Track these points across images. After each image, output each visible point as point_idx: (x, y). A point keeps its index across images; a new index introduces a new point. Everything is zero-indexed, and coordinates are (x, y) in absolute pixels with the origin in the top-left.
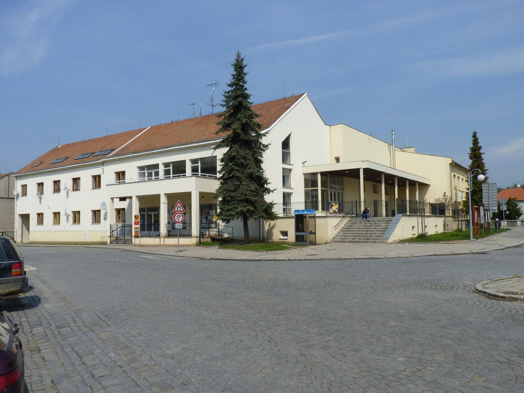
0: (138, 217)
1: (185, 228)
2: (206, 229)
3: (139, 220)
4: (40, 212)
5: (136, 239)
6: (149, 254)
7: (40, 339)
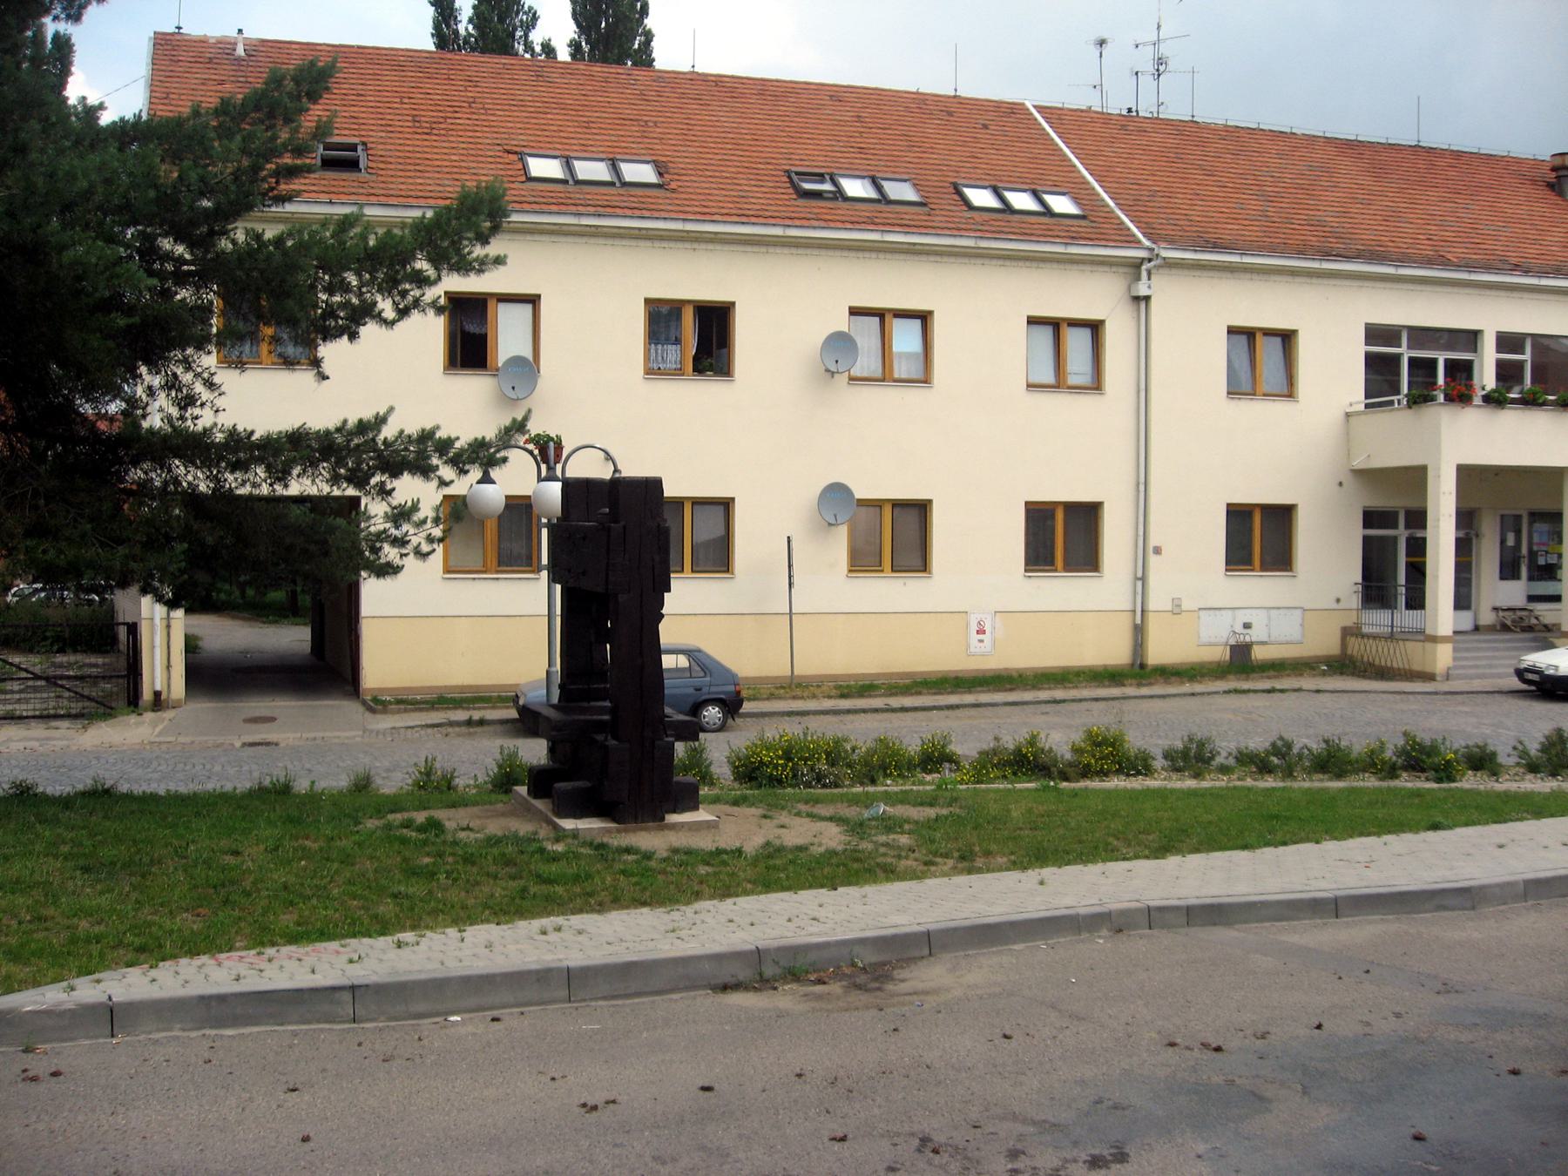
6: (1251, 694)
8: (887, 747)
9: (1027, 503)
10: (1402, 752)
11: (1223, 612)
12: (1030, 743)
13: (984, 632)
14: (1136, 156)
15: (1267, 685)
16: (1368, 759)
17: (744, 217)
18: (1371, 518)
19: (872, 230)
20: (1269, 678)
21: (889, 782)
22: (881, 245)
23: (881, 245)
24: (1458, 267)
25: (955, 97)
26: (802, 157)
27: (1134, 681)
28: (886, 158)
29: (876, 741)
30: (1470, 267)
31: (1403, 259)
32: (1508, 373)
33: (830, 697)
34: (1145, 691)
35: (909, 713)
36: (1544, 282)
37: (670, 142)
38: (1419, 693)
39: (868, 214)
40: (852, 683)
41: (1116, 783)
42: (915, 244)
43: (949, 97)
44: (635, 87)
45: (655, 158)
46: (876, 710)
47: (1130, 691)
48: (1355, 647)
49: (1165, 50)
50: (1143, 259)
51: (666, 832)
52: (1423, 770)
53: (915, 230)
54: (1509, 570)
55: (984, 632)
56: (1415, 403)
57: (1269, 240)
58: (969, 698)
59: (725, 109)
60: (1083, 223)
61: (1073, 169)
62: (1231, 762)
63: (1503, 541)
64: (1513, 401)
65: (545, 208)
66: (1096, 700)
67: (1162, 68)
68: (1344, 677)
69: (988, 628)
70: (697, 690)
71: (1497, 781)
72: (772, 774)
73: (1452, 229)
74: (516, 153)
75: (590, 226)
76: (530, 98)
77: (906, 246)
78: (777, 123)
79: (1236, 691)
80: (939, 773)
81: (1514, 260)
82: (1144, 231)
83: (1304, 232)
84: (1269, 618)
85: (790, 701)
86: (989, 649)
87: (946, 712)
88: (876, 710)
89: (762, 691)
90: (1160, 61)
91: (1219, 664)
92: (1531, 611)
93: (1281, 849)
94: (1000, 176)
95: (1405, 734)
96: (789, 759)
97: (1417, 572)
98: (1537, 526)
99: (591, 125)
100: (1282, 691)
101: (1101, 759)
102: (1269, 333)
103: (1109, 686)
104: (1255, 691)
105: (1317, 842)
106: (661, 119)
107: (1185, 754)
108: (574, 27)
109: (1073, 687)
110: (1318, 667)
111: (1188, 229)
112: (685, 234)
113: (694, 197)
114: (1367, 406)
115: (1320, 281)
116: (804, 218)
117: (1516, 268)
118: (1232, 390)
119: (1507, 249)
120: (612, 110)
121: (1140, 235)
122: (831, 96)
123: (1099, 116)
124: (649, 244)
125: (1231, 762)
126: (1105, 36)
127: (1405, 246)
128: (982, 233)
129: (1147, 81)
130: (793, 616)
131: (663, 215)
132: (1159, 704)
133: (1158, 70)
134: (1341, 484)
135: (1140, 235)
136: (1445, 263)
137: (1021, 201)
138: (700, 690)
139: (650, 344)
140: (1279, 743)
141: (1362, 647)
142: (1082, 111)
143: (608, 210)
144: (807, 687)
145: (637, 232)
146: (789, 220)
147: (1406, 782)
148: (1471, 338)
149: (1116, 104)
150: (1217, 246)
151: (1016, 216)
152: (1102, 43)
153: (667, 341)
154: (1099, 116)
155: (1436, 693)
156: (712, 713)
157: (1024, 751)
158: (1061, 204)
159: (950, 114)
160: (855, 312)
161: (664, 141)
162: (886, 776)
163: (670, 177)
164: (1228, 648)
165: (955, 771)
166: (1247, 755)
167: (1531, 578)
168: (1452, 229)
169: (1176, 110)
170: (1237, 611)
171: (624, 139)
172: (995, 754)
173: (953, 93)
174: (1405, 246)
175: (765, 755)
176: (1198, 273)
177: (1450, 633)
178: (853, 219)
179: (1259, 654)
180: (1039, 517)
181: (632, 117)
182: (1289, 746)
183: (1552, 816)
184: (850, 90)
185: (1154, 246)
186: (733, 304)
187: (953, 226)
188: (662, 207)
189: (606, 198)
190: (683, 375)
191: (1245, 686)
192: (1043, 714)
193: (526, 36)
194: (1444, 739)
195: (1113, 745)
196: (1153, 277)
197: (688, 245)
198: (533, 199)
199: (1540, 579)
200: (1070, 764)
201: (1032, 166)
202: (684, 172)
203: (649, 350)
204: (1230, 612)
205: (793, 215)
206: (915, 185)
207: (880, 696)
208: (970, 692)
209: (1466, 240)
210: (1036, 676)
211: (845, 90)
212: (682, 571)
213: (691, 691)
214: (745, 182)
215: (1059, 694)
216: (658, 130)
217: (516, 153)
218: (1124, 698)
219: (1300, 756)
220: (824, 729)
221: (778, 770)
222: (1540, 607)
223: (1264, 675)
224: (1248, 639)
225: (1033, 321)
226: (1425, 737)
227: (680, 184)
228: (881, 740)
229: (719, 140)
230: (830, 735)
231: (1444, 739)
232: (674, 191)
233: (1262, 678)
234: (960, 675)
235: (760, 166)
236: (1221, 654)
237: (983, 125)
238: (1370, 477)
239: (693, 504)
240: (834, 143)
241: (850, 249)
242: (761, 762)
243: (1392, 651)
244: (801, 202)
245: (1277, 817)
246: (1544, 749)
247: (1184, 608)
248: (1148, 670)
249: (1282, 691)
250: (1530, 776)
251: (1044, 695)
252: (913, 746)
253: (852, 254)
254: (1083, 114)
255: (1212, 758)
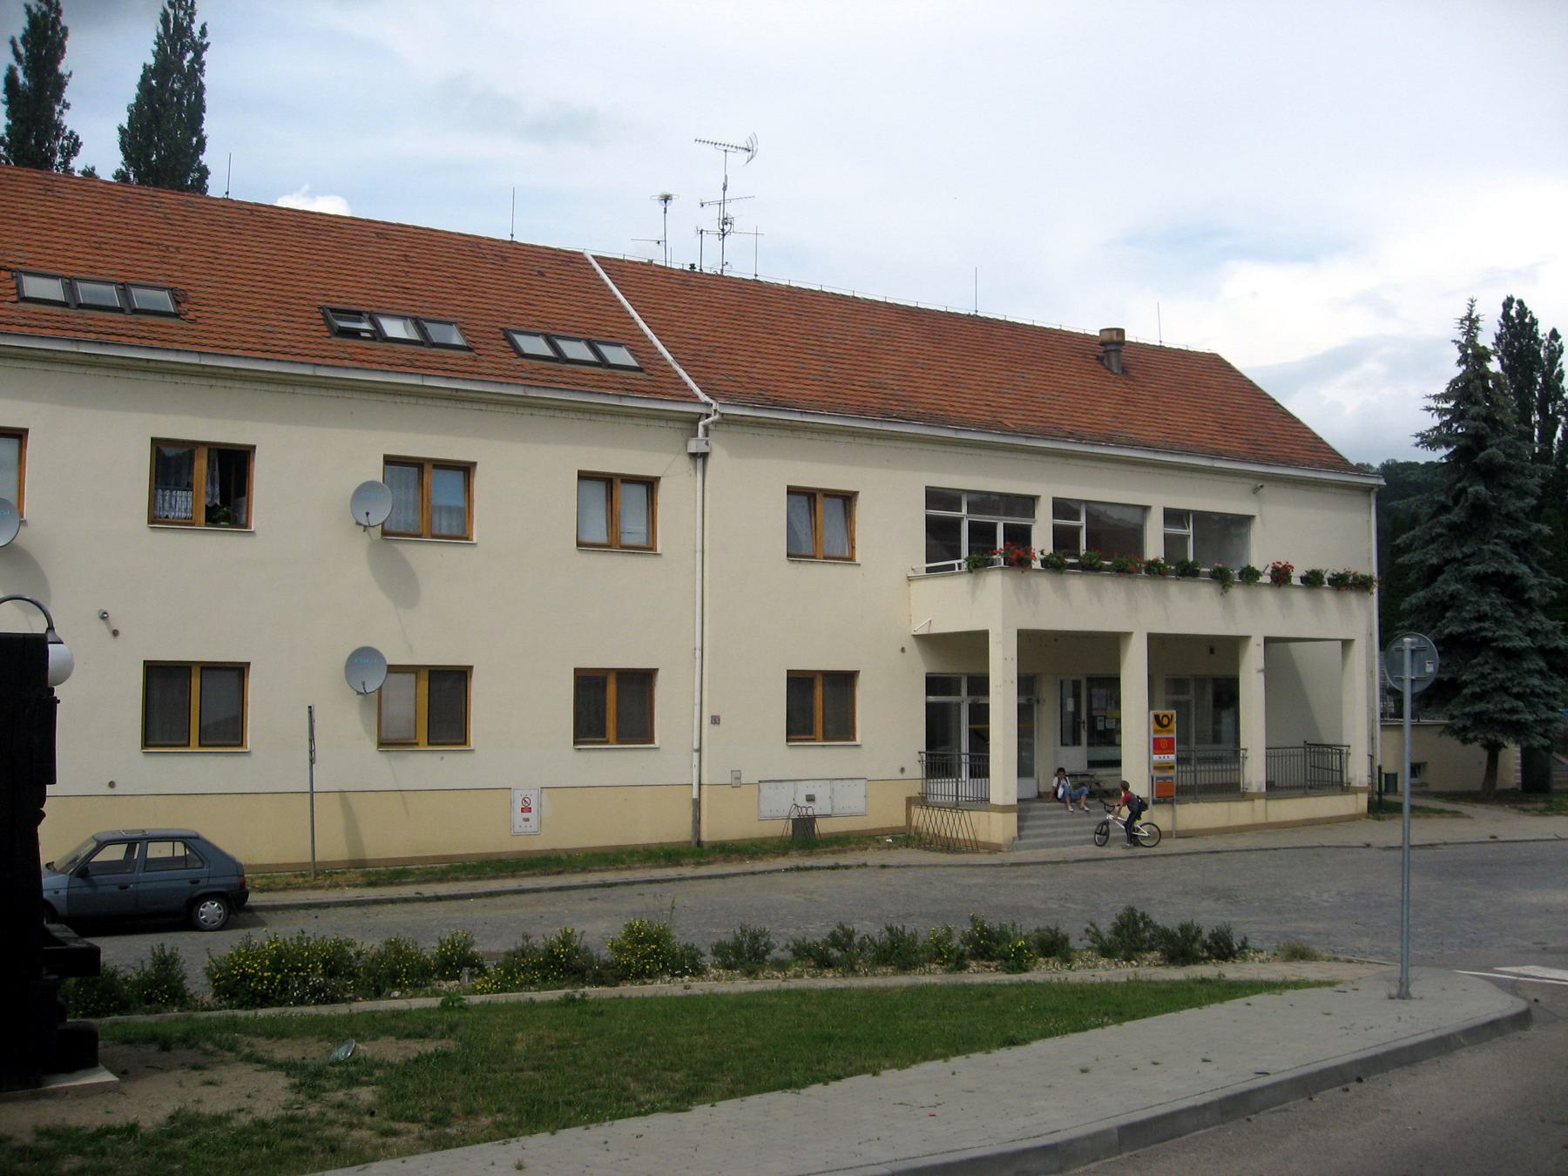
0: (1170, 720)
1: (1185, 759)
2: (1216, 762)
3: (1170, 731)
4: (716, 727)
5: (1556, 787)
6: (814, 873)
7: (861, 1166)
8: (399, 952)
9: (576, 670)
10: (969, 939)
11: (785, 784)
12: (562, 942)
13: (529, 810)
14: (698, 312)
15: (829, 860)
16: (934, 949)
17: (269, 354)
18: (934, 684)
19: (411, 373)
20: (833, 853)
21: (396, 993)
22: (420, 390)
23: (420, 390)
24: (1015, 434)
25: (512, 242)
26: (340, 294)
27: (692, 861)
28: (432, 300)
29: (386, 943)
30: (1028, 434)
31: (964, 425)
32: (1064, 539)
33: (355, 886)
34: (703, 871)
35: (444, 903)
36: (1097, 450)
37: (193, 270)
38: (986, 865)
39: (409, 357)
40: (383, 869)
41: (665, 987)
42: (457, 390)
43: (504, 242)
44: (160, 210)
45: (172, 285)
46: (406, 900)
47: (687, 871)
48: (920, 817)
49: (730, 210)
50: (701, 414)
51: (43, 1101)
52: (991, 959)
53: (460, 375)
54: (1070, 736)
55: (529, 810)
56: (976, 567)
57: (830, 400)
58: (511, 884)
59: (258, 239)
60: (639, 375)
61: (631, 321)
62: (787, 955)
63: (1062, 706)
64: (1072, 566)
65: (37, 331)
66: (650, 882)
67: (727, 228)
68: (910, 850)
69: (534, 806)
70: (192, 882)
71: (1070, 968)
72: (256, 989)
73: (1009, 396)
74: (9, 270)
75: (90, 354)
76: (35, 213)
77: (448, 392)
78: (316, 258)
79: (798, 869)
80: (459, 979)
81: (1068, 428)
82: (701, 386)
83: (865, 394)
84: (833, 790)
85: (309, 892)
86: (535, 828)
87: (487, 901)
88: (406, 900)
89: (277, 880)
90: (725, 221)
91: (781, 839)
92: (1092, 776)
93: (834, 1085)
94: (553, 324)
95: (973, 919)
96: (279, 971)
97: (980, 739)
98: (1095, 691)
99: (103, 246)
100: (847, 867)
101: (643, 958)
102: (830, 494)
103: (666, 866)
104: (819, 868)
105: (875, 1074)
106: (184, 245)
107: (737, 949)
108: (120, 157)
109: (626, 869)
110: (884, 840)
111: (748, 386)
112: (200, 369)
113: (214, 329)
114: (928, 570)
115: (881, 442)
116: (336, 358)
117: (1069, 436)
118: (793, 552)
119: (1062, 417)
120: (129, 232)
121: (697, 390)
122: (377, 234)
123: (662, 270)
124: (158, 377)
125: (787, 955)
126: (668, 192)
127: (964, 411)
128: (530, 382)
129: (712, 241)
130: (308, 790)
131: (177, 346)
132: (718, 883)
133: (723, 230)
134: (903, 650)
135: (697, 390)
136: (1004, 430)
137: (576, 350)
138: (197, 882)
139: (156, 489)
140: (839, 932)
141: (928, 819)
142: (643, 264)
143: (114, 338)
144: (330, 875)
145: (144, 364)
146: (318, 360)
147: (979, 975)
148: (1027, 504)
149: (679, 262)
150: (777, 405)
151: (569, 366)
152: (666, 199)
153: (178, 486)
154: (662, 270)
155: (1002, 865)
156: (211, 910)
157: (556, 951)
158: (618, 355)
159: (505, 259)
160: (390, 461)
161: (185, 268)
162: (395, 986)
163: (189, 306)
164: (791, 821)
165: (478, 976)
166: (804, 949)
167: (1090, 744)
168: (1009, 396)
169: (741, 268)
170: (798, 783)
171: (139, 263)
172: (524, 956)
173: (509, 239)
174: (964, 411)
175: (249, 966)
176: (757, 431)
177: (1015, 802)
178: (391, 361)
179: (822, 827)
180: (589, 684)
181: (151, 241)
182: (850, 935)
183: (1133, 1017)
184: (399, 228)
185: (711, 401)
186: (254, 447)
187: (500, 373)
188: (175, 338)
189: (112, 325)
190: (193, 524)
191: (809, 862)
192: (590, 900)
193: (66, 162)
194: (1014, 925)
195: (656, 942)
196: (710, 433)
197: (204, 381)
198: (23, 322)
199: (1100, 744)
200: (607, 966)
201: (588, 316)
202: (204, 302)
203: (156, 496)
204: (792, 784)
205: (325, 353)
206: (461, 329)
207: (413, 883)
208: (513, 877)
209: (1023, 407)
210: (586, 855)
211: (395, 228)
212: (188, 745)
213: (187, 884)
214: (275, 317)
215: (610, 876)
216: (181, 256)
217: (9, 270)
218: (680, 879)
219: (862, 947)
220: (322, 930)
221: (263, 984)
222: (1100, 773)
223: (827, 850)
224: (810, 812)
225: (584, 476)
226: (993, 923)
227: (199, 314)
228: (391, 943)
229: (248, 271)
230: (331, 938)
231: (1014, 925)
232: (192, 321)
233: (826, 852)
234: (503, 857)
235: (292, 301)
236: (782, 828)
237: (539, 272)
238: (931, 642)
239: (202, 668)
240: (376, 281)
241: (386, 392)
242: (244, 976)
243: (957, 822)
244: (337, 340)
245: (829, 1039)
246: (1118, 930)
247: (744, 780)
248: (706, 847)
249: (847, 867)
250: (1103, 961)
251: (593, 878)
252: (429, 949)
253: (389, 398)
254: (645, 267)
255: (767, 951)
